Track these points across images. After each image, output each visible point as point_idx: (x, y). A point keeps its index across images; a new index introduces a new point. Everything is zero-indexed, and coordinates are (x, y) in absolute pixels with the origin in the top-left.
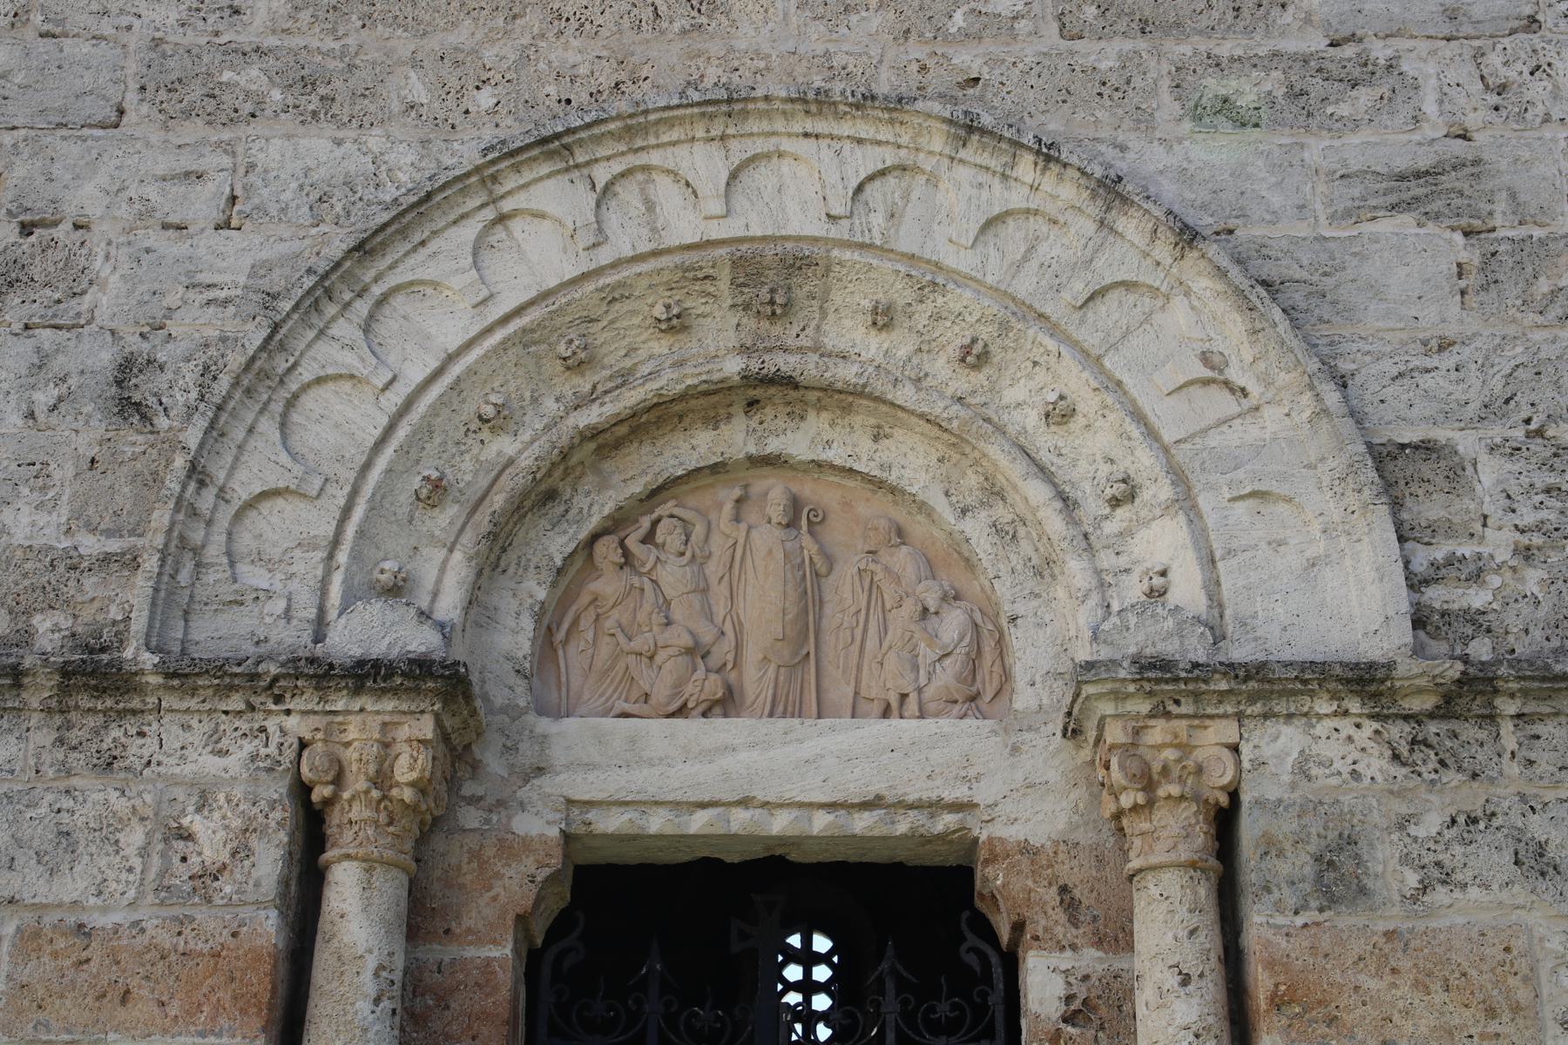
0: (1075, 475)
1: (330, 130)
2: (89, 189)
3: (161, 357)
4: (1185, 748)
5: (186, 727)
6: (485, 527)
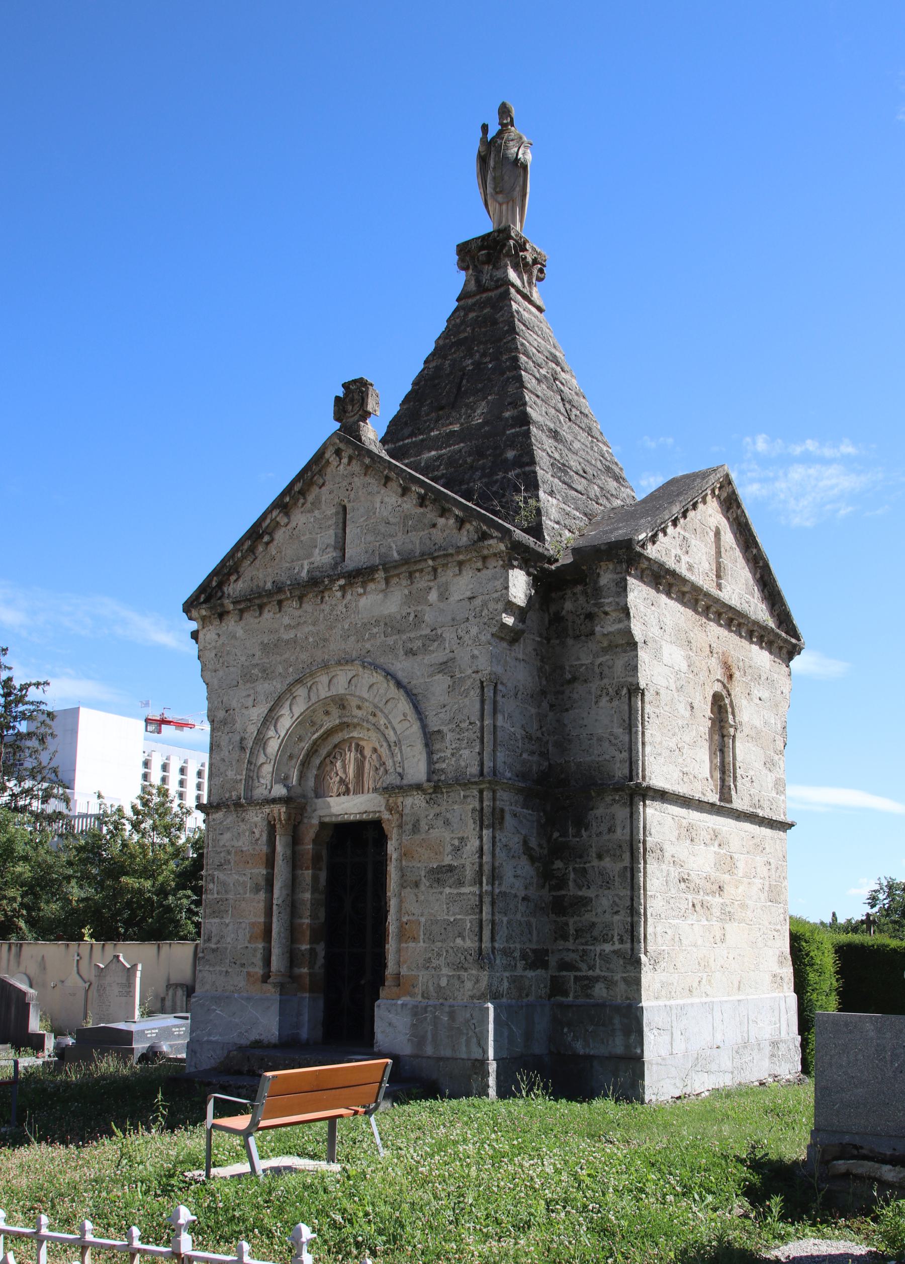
1: (268, 682)
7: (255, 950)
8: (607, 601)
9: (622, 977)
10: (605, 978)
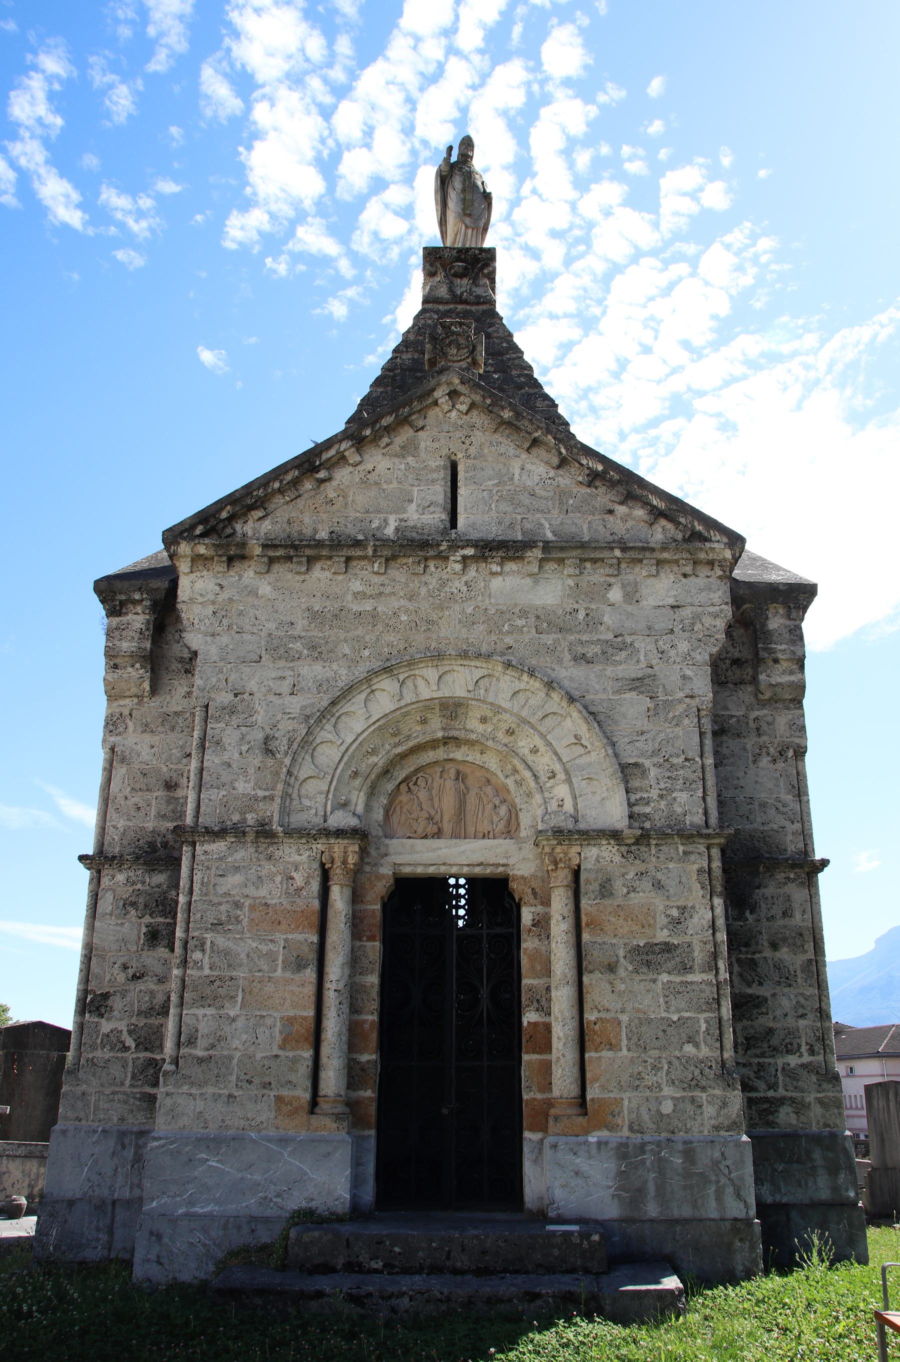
0: (538, 769)
1: (321, 663)
2: (253, 682)
3: (276, 735)
4: (566, 854)
5: (290, 847)
6: (370, 784)
7: (295, 1061)
8: (779, 647)
9: (817, 1098)
10: (793, 1100)
